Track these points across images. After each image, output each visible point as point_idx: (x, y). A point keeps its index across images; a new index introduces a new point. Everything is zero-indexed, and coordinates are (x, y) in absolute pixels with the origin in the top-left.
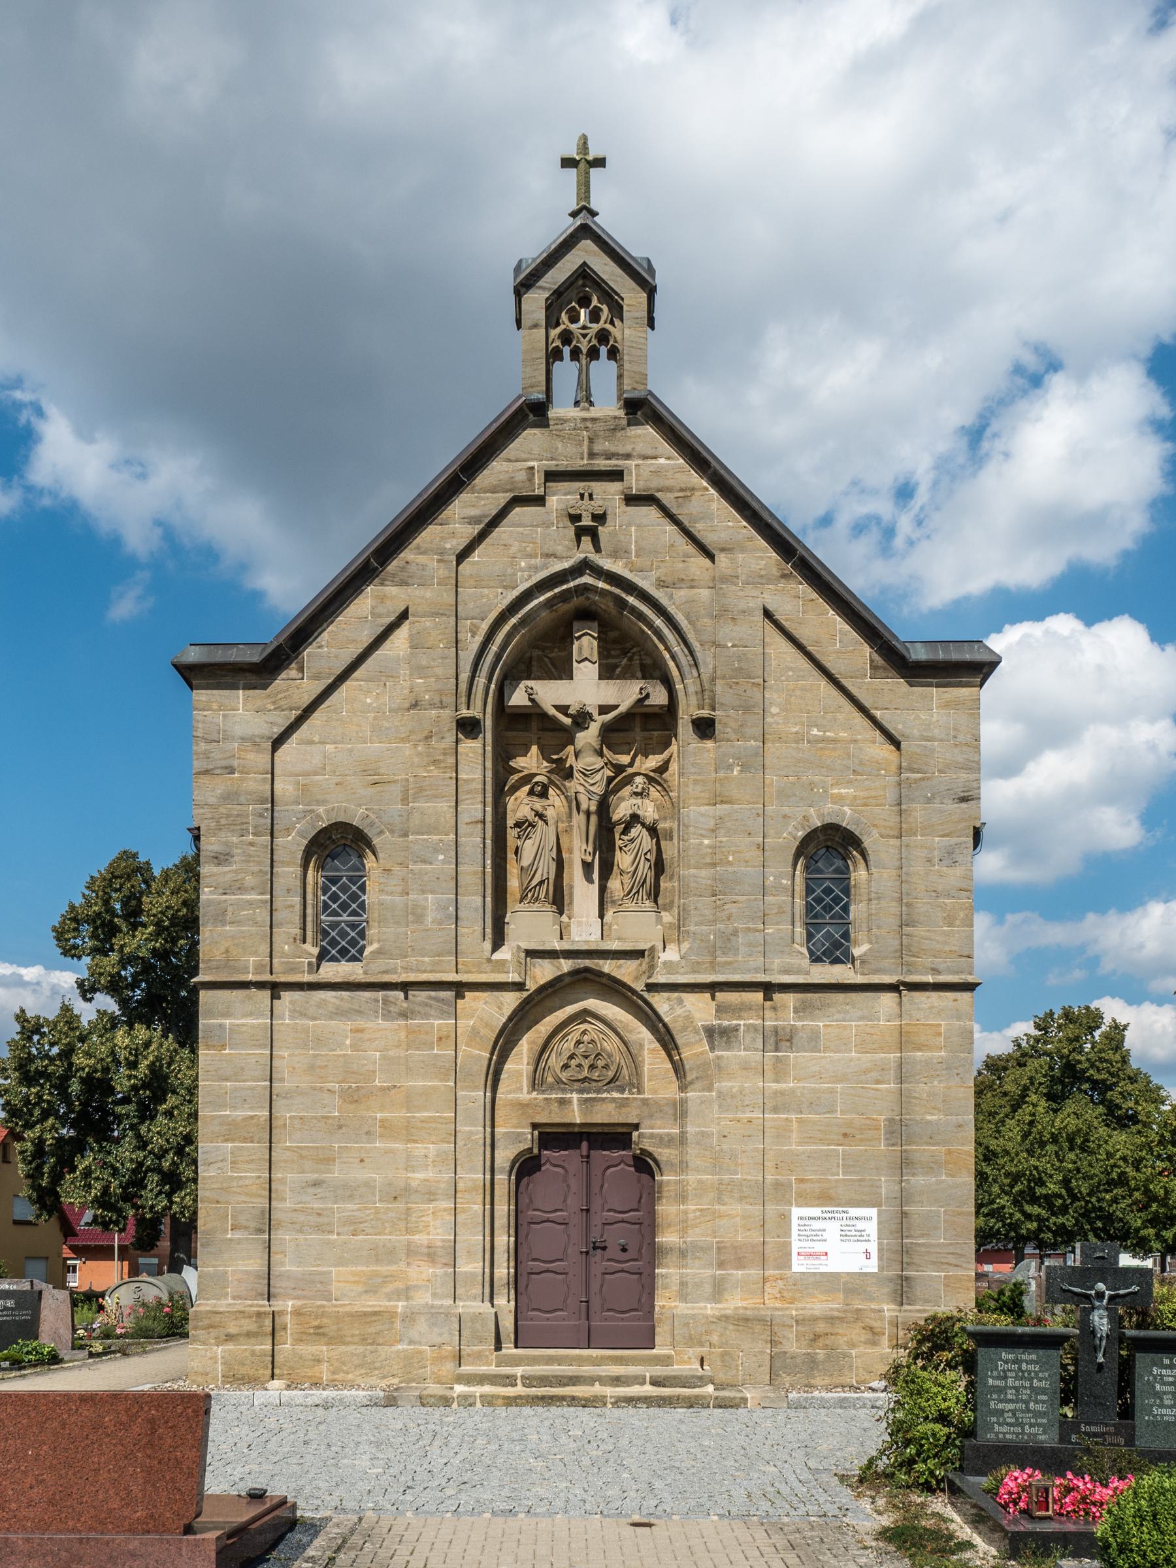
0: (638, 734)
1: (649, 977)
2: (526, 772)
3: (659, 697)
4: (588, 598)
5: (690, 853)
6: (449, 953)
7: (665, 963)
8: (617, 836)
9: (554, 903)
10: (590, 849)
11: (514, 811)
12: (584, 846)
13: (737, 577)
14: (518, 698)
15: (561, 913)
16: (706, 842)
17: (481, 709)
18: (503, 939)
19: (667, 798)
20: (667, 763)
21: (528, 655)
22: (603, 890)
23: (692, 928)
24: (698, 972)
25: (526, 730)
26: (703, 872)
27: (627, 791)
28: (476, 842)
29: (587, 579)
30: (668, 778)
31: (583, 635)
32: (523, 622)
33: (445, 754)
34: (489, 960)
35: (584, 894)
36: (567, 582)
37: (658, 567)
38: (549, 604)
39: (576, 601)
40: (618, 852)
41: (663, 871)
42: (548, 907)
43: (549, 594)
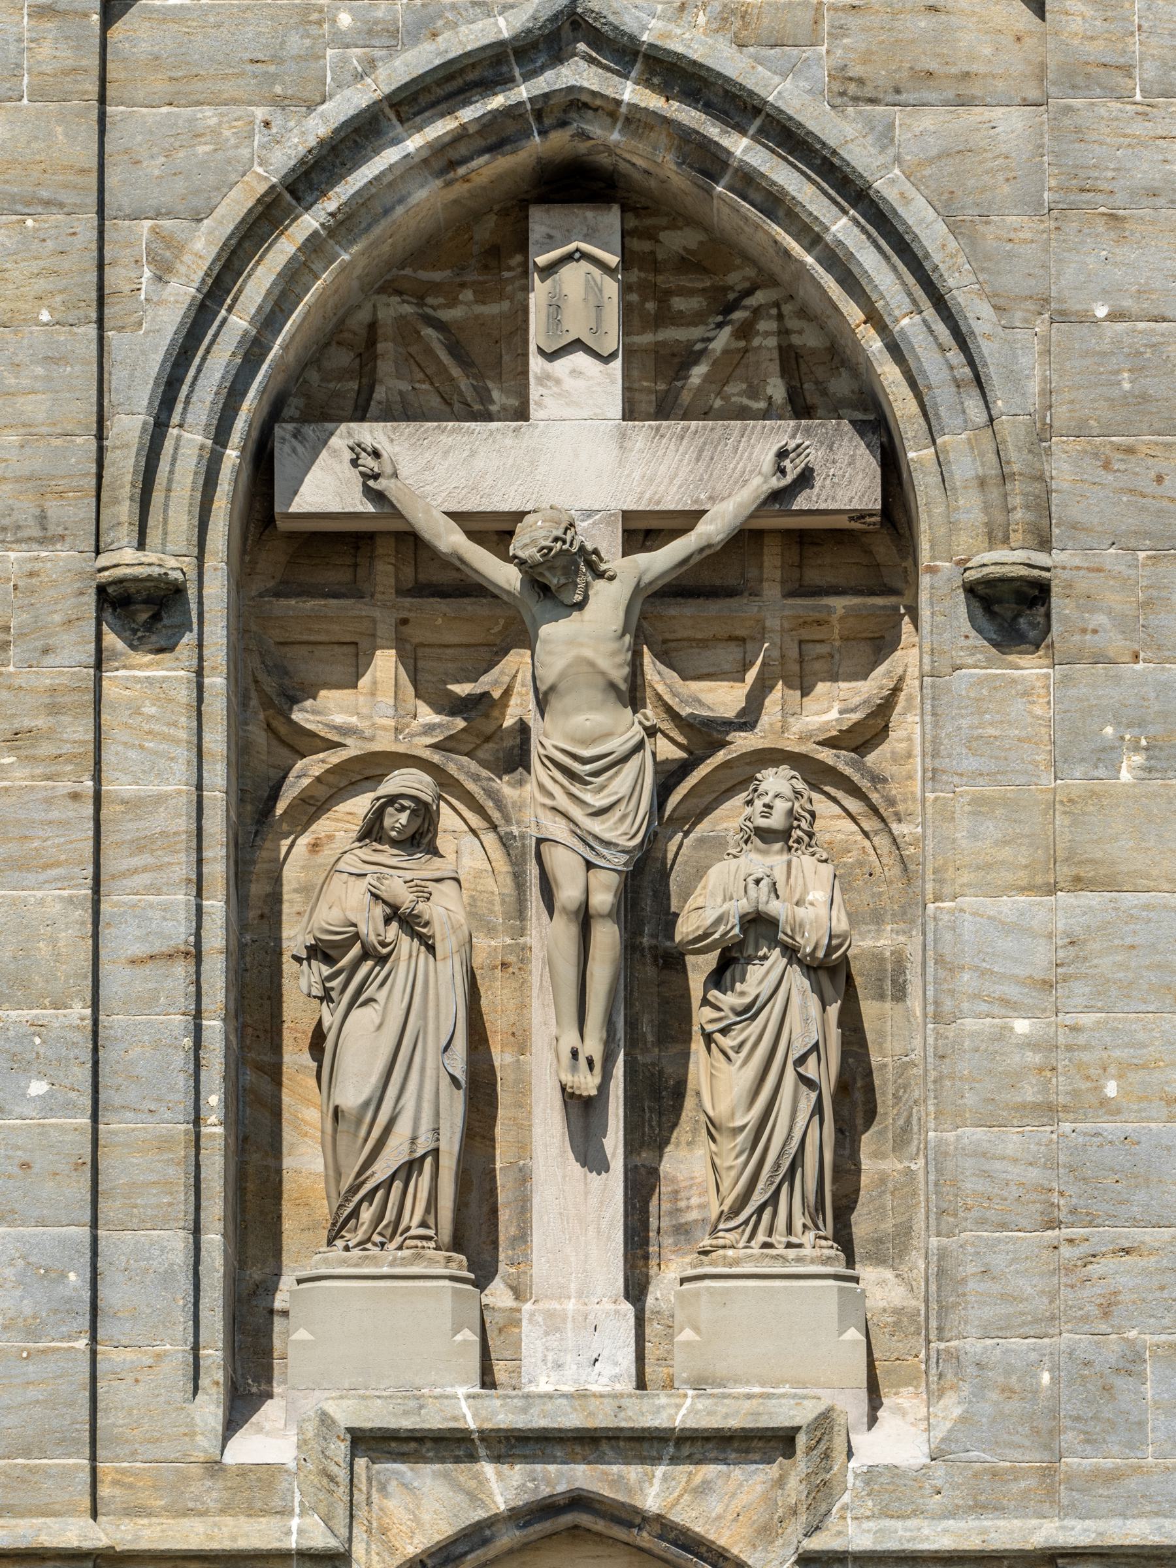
0: (773, 609)
1: (813, 1530)
2: (354, 748)
3: (846, 481)
4: (584, 136)
5: (964, 1068)
6: (64, 1444)
7: (871, 1474)
8: (696, 982)
9: (457, 1244)
10: (593, 1046)
11: (313, 893)
12: (570, 1038)
13: (1127, 70)
14: (324, 488)
15: (482, 1274)
16: (1022, 1026)
17: (188, 543)
18: (266, 1374)
19: (881, 841)
20: (883, 710)
21: (364, 316)
22: (641, 1187)
23: (973, 1346)
24: (998, 1509)
25: (354, 591)
26: (1012, 1140)
27: (730, 817)
28: (164, 1028)
29: (578, 73)
30: (889, 769)
31: (569, 258)
32: (344, 225)
33: (54, 709)
34: (214, 1467)
35: (568, 1211)
36: (504, 82)
37: (840, 31)
38: (443, 160)
39: (536, 146)
40: (697, 1045)
41: (871, 1115)
42: (437, 1262)
43: (440, 128)
